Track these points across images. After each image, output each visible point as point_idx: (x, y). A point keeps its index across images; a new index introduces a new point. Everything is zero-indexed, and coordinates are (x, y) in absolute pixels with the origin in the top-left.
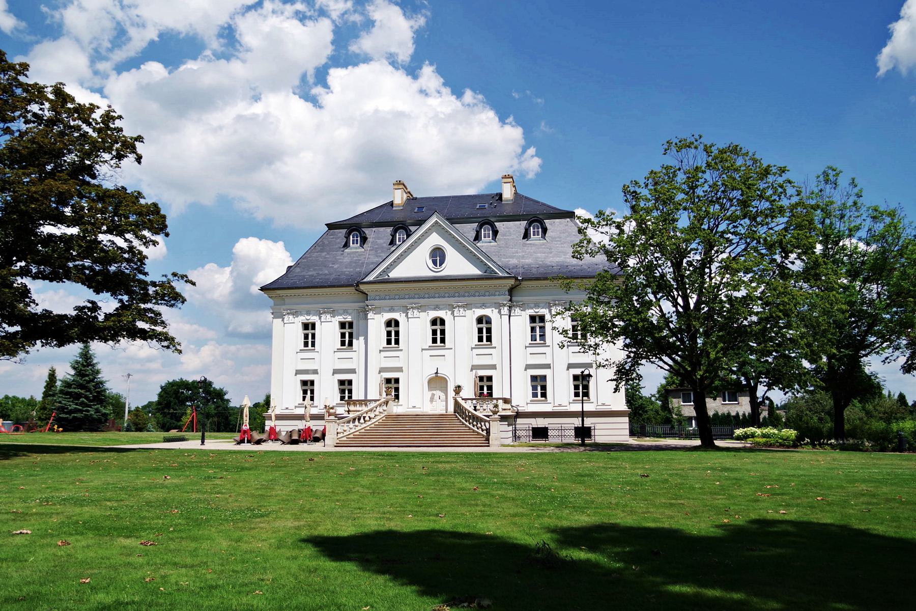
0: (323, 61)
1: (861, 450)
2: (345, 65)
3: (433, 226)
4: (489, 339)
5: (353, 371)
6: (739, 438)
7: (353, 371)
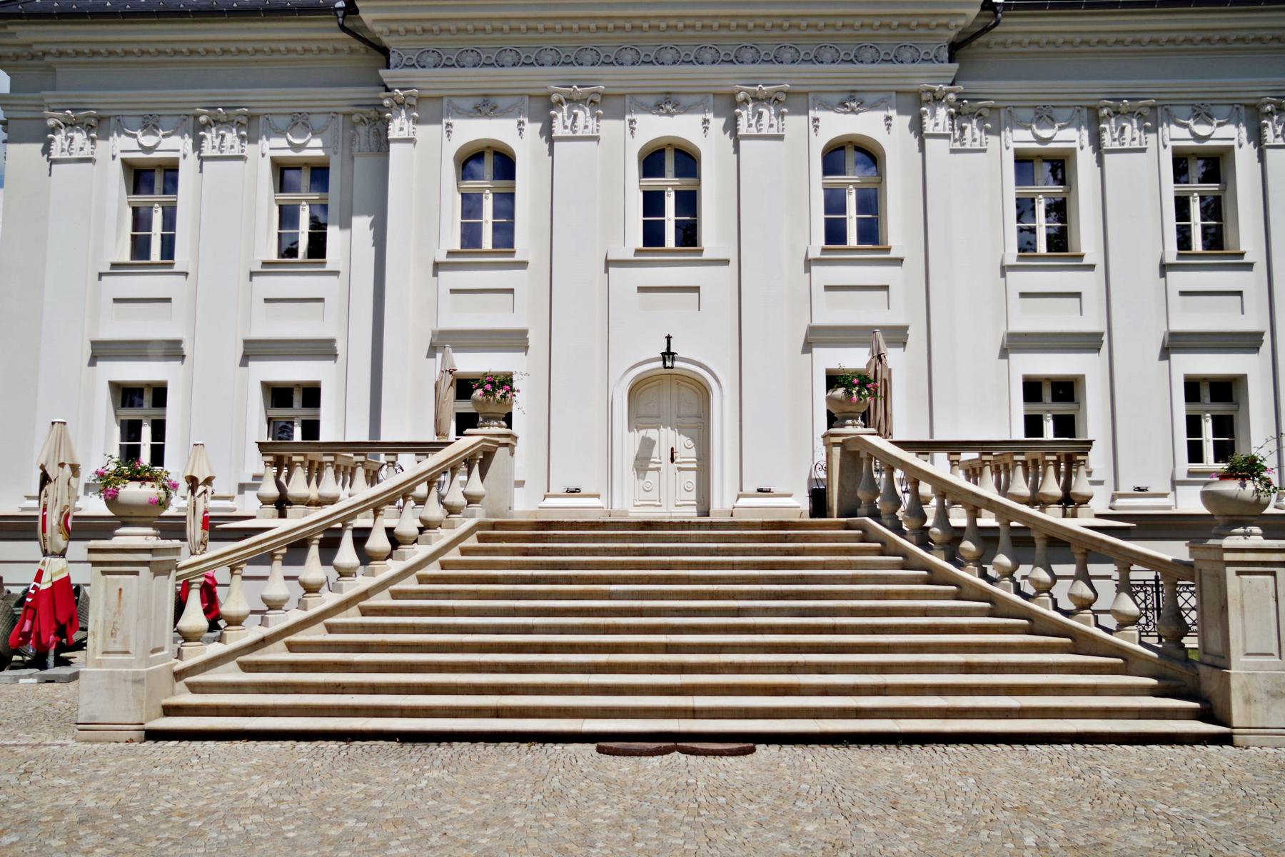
5: (323, 349)
7: (323, 349)
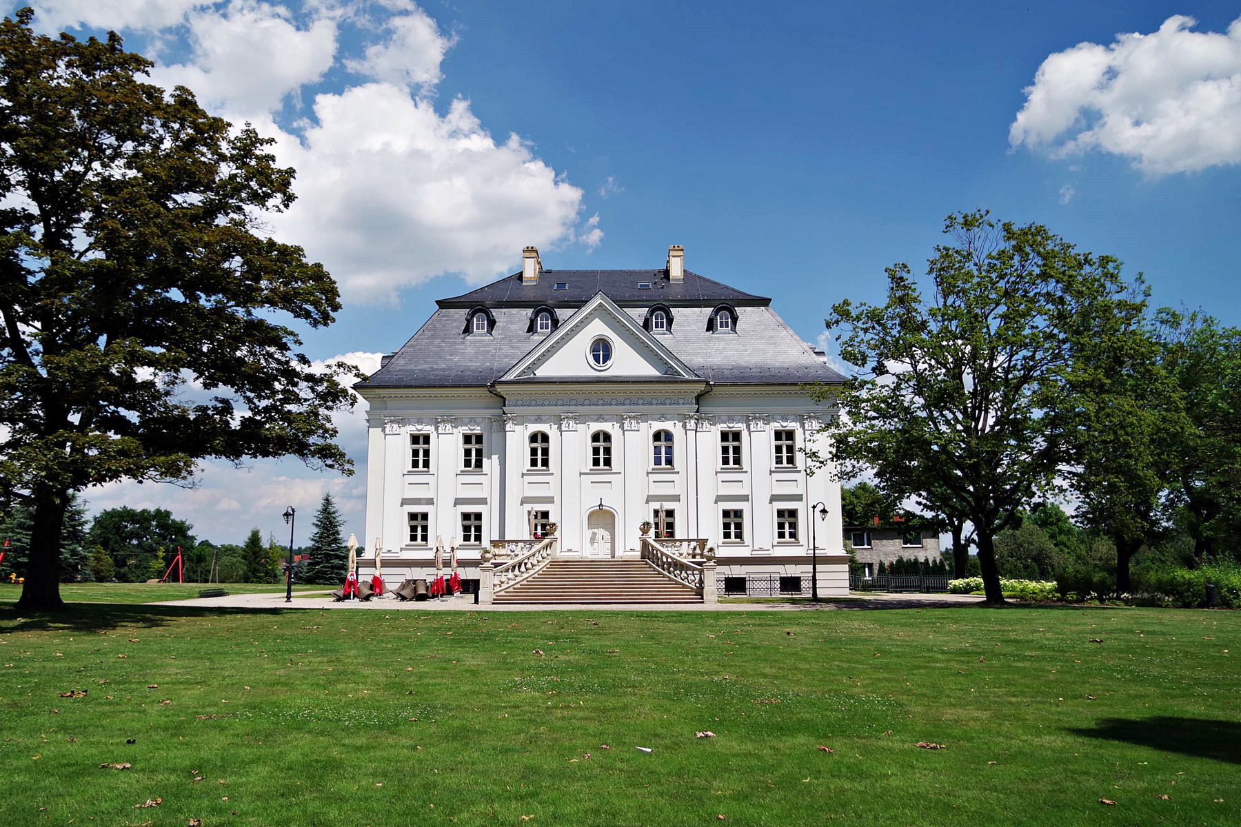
0: (316, 79)
1: (1160, 606)
2: (339, 91)
3: (595, 309)
4: (545, 463)
5: (483, 501)
6: (955, 591)
7: (483, 501)
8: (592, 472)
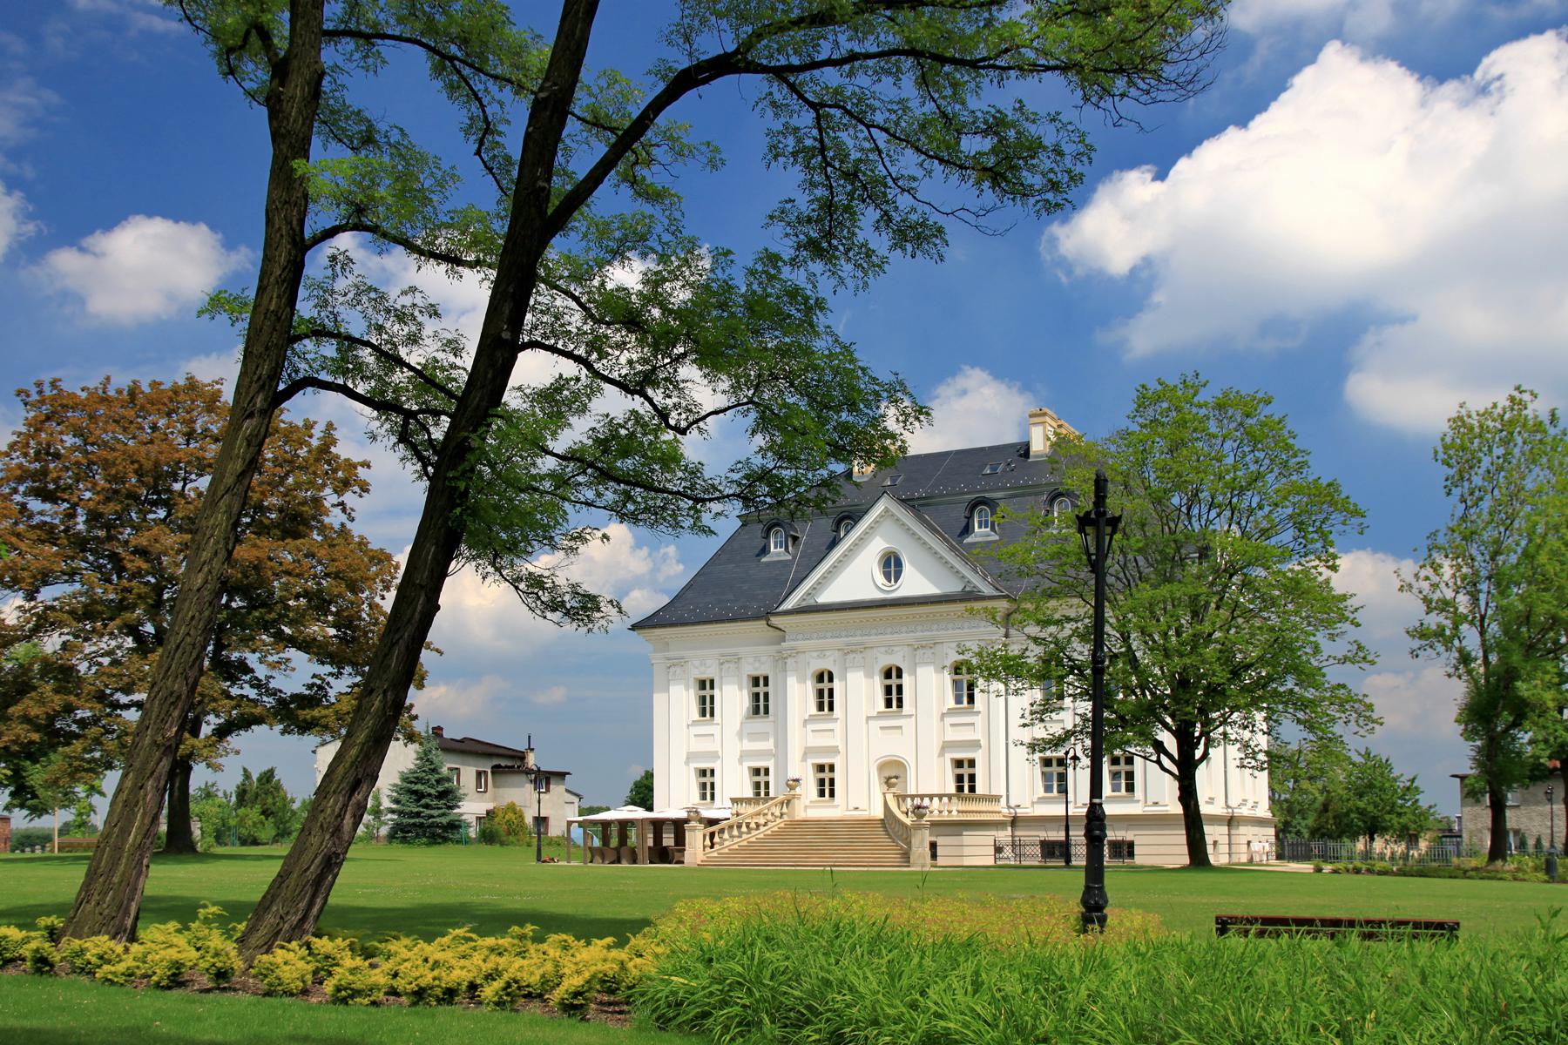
3: (881, 516)
8: (880, 716)
